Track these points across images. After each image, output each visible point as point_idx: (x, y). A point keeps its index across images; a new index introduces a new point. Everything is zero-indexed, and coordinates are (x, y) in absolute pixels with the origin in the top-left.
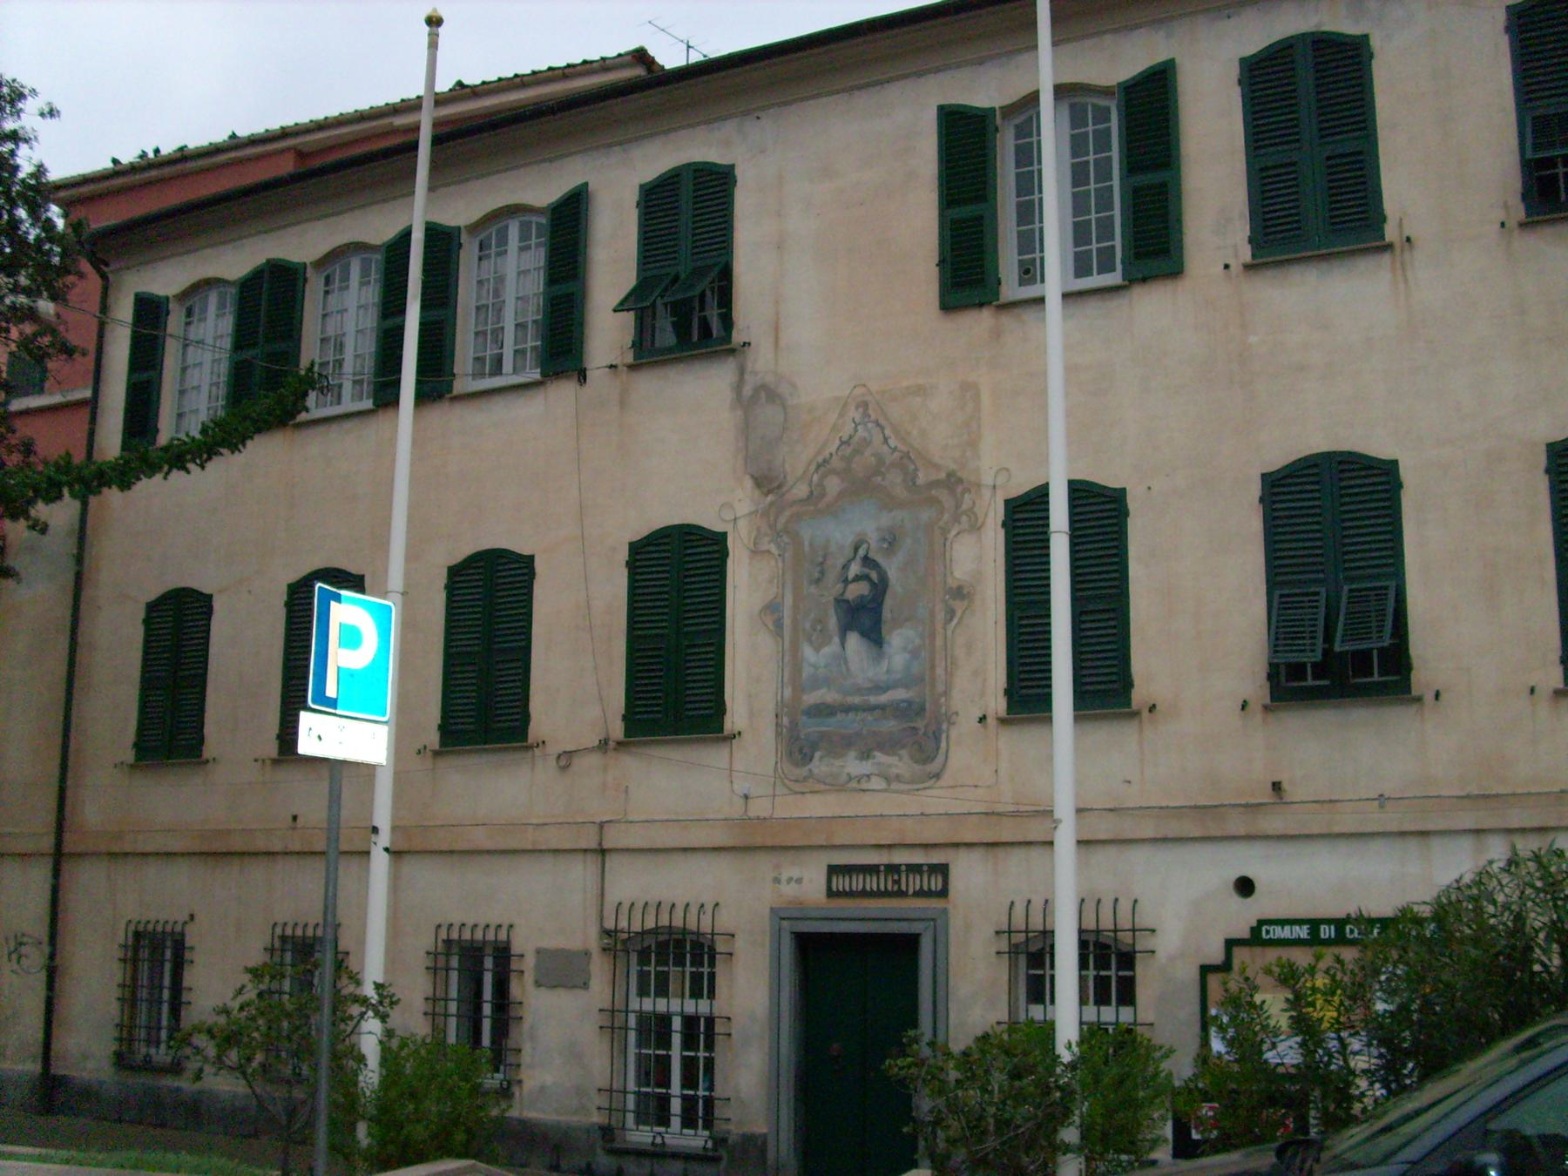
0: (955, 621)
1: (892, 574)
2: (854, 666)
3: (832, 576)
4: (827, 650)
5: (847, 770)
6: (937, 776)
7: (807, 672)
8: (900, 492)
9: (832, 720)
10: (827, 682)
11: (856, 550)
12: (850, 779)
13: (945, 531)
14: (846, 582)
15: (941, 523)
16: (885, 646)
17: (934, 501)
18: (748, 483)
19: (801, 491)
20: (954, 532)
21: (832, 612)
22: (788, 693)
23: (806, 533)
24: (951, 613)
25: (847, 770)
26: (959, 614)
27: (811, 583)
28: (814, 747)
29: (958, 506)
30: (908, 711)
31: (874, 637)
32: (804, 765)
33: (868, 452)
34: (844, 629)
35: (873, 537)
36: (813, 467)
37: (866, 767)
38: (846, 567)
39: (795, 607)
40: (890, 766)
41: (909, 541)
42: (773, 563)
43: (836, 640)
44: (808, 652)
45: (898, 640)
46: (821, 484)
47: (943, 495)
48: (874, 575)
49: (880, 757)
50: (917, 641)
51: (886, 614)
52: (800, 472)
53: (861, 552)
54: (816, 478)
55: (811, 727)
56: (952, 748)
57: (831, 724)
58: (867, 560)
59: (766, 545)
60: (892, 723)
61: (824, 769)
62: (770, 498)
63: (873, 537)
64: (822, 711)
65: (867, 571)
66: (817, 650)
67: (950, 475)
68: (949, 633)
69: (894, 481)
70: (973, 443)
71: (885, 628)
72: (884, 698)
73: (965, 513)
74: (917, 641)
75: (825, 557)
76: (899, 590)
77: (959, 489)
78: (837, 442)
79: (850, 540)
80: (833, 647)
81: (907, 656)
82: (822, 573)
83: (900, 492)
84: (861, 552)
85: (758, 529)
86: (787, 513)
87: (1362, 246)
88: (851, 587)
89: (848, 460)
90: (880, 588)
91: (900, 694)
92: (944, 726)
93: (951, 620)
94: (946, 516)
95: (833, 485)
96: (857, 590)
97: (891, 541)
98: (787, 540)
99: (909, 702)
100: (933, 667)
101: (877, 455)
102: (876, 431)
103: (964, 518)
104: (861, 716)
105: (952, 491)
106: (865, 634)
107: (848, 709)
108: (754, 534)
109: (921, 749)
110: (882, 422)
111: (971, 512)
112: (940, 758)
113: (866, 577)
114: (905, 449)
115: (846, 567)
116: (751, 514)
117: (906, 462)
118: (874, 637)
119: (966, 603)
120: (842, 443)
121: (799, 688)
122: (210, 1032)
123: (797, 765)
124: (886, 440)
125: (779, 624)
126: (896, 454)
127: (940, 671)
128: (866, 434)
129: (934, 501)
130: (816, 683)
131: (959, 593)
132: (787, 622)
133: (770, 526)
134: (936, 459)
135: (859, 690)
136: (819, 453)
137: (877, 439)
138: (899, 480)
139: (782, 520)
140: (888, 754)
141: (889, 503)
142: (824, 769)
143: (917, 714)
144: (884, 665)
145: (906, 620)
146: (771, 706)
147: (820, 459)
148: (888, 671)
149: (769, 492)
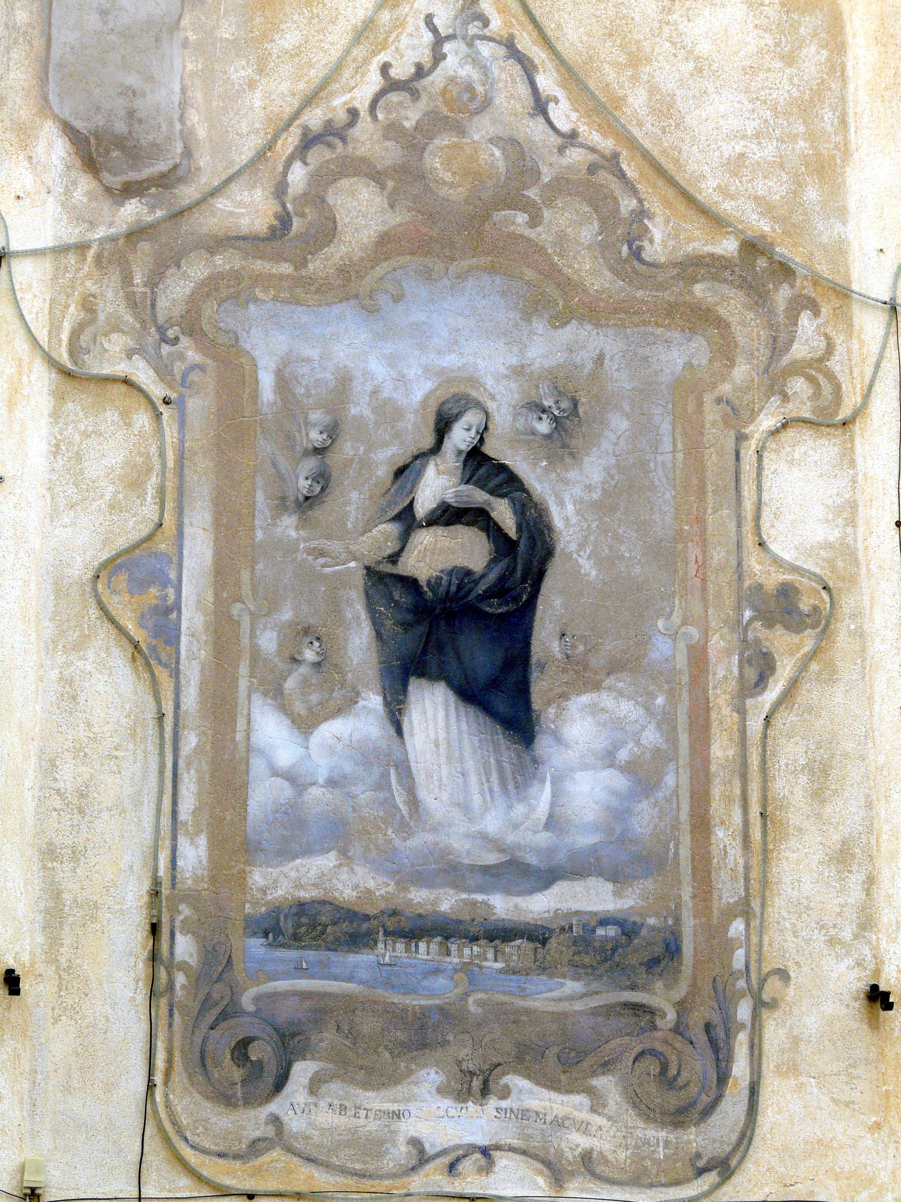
0: (771, 695)
1: (565, 517)
2: (436, 799)
3: (354, 500)
4: (333, 729)
5: (410, 1127)
6: (724, 1167)
7: (264, 795)
8: (592, 273)
9: (362, 959)
10: (339, 835)
11: (443, 426)
12: (422, 1156)
13: (737, 415)
14: (406, 519)
15: (726, 388)
16: (543, 744)
17: (702, 318)
18: (54, 149)
19: (248, 208)
20: (767, 421)
21: (356, 609)
22: (194, 855)
23: (268, 344)
24: (761, 666)
25: (410, 1127)
26: (785, 670)
27: (281, 505)
28: (290, 1043)
29: (778, 345)
30: (626, 953)
31: (506, 702)
32: (251, 1100)
33: (481, 129)
34: (403, 671)
35: (503, 402)
36: (290, 141)
37: (475, 1124)
38: (405, 473)
39: (222, 572)
40: (560, 1123)
41: (619, 424)
42: (142, 420)
43: (374, 701)
44: (271, 732)
45: (580, 727)
46: (315, 195)
47: (732, 305)
48: (504, 514)
49: (526, 1093)
50: (651, 736)
51: (545, 640)
52: (244, 154)
53: (460, 437)
54: (298, 175)
55: (278, 979)
56: (774, 1088)
57: (350, 974)
58: (477, 462)
59: (113, 357)
60: (572, 986)
61: (326, 1118)
62: (132, 211)
63: (503, 402)
64: (311, 926)
65: (479, 496)
66: (305, 725)
67: (752, 247)
68: (755, 725)
69: (571, 233)
70: (826, 167)
71: (540, 687)
72: (538, 906)
73: (797, 369)
74: (651, 736)
75: (333, 431)
76: (588, 567)
77: (783, 295)
78: (373, 82)
79: (418, 393)
80: (365, 720)
81: (619, 781)
82: (323, 478)
83: (592, 273)
84: (460, 437)
85: (88, 305)
86: (197, 270)
87: (177, 1044)
88: (424, 538)
89: (414, 142)
90: (526, 556)
91: (595, 897)
92: (744, 1012)
93: (762, 682)
94: (741, 371)
95: (363, 213)
96: (459, 552)
97: (565, 421)
98: (193, 356)
99: (629, 929)
100: (702, 825)
101: (512, 145)
102: (506, 73)
103: (798, 385)
104: (462, 953)
105: (758, 296)
106: (470, 694)
107: (415, 930)
108: (73, 314)
109: (666, 1078)
110: (526, 43)
111: (817, 368)
112: (732, 1108)
113: (478, 517)
114: (607, 144)
115: (405, 473)
116: (60, 250)
117: (617, 179)
118: (506, 702)
119: (807, 641)
120: (392, 85)
121: (235, 846)
122: (483, 434)
123: (225, 1099)
124: (540, 106)
125: (164, 621)
126: (575, 156)
127: (724, 837)
128: (467, 72)
129: (702, 318)
130: (295, 833)
131: (784, 606)
132: (192, 619)
133: (132, 302)
134: (707, 191)
135: (452, 872)
136: (310, 100)
137: (510, 95)
138: (588, 233)
139: (176, 292)
140: (553, 1085)
141: (550, 297)
142: (326, 1118)
143: (652, 963)
144: (542, 798)
145: (615, 667)
146: (133, 895)
147: (315, 118)
148: (552, 822)
149: (128, 191)
